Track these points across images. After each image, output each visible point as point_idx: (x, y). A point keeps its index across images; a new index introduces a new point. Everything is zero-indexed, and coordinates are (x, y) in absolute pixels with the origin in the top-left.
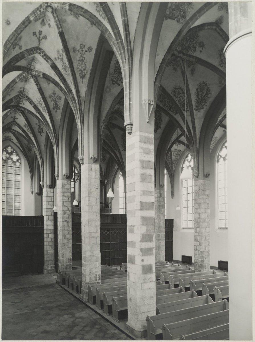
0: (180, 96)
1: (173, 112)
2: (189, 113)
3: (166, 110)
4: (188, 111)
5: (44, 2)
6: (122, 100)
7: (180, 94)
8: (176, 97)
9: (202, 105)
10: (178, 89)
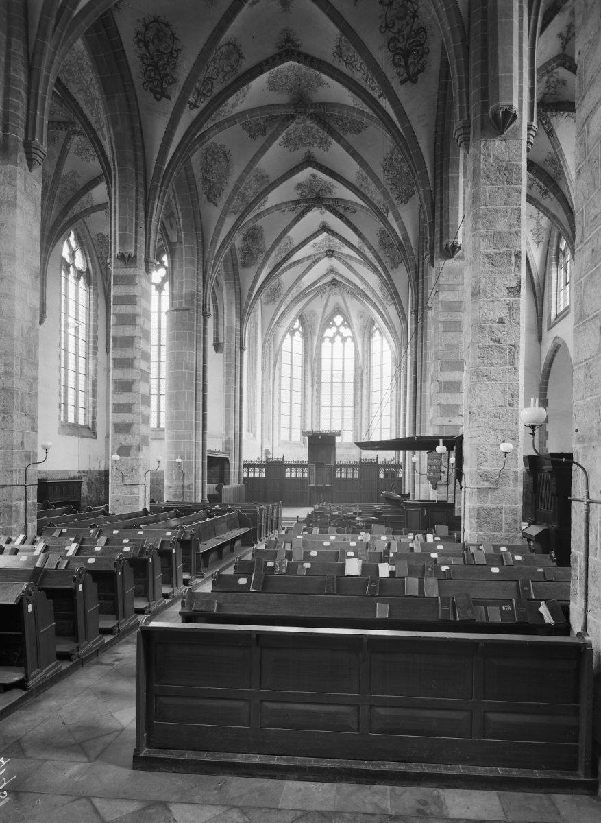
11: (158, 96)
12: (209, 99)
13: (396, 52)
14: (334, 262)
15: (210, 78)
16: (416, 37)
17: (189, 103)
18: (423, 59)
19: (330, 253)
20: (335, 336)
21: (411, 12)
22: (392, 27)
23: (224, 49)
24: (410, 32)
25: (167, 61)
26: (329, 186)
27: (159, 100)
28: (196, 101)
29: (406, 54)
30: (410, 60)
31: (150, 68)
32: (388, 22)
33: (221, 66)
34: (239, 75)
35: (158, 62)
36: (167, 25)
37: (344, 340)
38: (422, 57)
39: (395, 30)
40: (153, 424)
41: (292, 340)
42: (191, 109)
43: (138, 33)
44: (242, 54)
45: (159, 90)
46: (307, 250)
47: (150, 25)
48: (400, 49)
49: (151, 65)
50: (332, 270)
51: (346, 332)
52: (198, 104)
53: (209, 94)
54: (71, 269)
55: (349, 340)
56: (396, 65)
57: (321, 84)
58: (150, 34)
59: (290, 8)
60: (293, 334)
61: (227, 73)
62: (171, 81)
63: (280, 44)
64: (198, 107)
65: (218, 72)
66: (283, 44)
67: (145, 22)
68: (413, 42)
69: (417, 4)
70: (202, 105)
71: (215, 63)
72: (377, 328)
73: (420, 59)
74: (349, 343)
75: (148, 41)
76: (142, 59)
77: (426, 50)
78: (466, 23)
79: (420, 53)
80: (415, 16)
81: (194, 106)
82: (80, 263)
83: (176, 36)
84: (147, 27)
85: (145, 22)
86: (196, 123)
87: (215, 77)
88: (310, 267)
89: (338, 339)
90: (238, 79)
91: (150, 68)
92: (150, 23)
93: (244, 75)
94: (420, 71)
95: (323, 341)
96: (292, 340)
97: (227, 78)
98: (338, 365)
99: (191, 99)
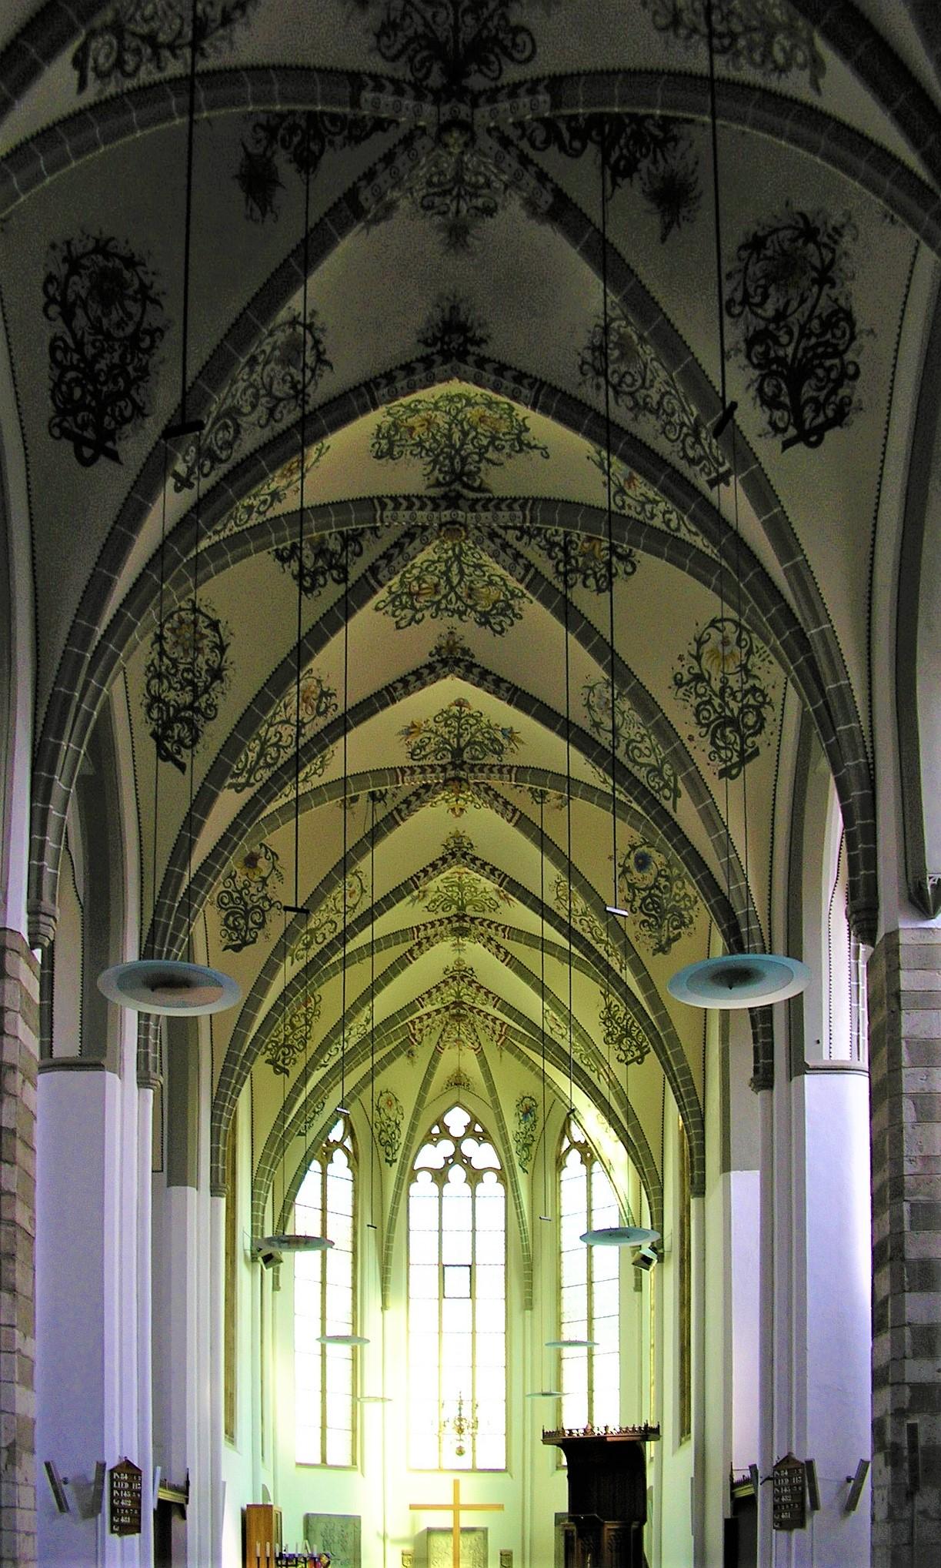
11: (87, 452)
12: (223, 469)
13: (766, 366)
14: (476, 954)
16: (823, 334)
17: (176, 475)
18: (843, 392)
19: (461, 925)
20: (447, 1166)
21: (814, 268)
22: (761, 305)
23: (281, 337)
24: (810, 318)
25: (122, 357)
26: (499, 736)
27: (86, 462)
28: (190, 471)
29: (796, 374)
30: (807, 391)
31: (71, 375)
32: (751, 290)
33: (266, 380)
35: (96, 358)
36: (130, 262)
37: (474, 1177)
38: (839, 383)
39: (769, 310)
41: (324, 1174)
42: (178, 490)
43: (50, 279)
44: (324, 352)
45: (89, 434)
46: (402, 915)
47: (85, 262)
48: (780, 361)
49: (73, 368)
50: (461, 974)
51: (483, 1155)
53: (223, 456)
55: (490, 1178)
56: (770, 402)
57: (521, 443)
58: (80, 286)
59: (469, 239)
60: (327, 1158)
61: (280, 400)
62: (127, 413)
63: (430, 334)
65: (256, 396)
66: (439, 335)
67: (69, 251)
68: (818, 345)
69: (833, 251)
70: (205, 484)
71: (252, 372)
72: (574, 1144)
73: (834, 392)
74: (491, 1185)
75: (74, 304)
76: (53, 349)
77: (851, 370)
78: (724, 312)
79: (834, 375)
80: (825, 277)
81: (183, 483)
83: (152, 293)
84: (74, 264)
85: (69, 251)
86: (185, 529)
87: (246, 409)
88: (402, 963)
89: (457, 1173)
91: (71, 375)
92: (83, 255)
93: (326, 407)
94: (830, 424)
95: (413, 1178)
96: (324, 1174)
97: (278, 416)
98: (457, 1250)
99: (181, 468)
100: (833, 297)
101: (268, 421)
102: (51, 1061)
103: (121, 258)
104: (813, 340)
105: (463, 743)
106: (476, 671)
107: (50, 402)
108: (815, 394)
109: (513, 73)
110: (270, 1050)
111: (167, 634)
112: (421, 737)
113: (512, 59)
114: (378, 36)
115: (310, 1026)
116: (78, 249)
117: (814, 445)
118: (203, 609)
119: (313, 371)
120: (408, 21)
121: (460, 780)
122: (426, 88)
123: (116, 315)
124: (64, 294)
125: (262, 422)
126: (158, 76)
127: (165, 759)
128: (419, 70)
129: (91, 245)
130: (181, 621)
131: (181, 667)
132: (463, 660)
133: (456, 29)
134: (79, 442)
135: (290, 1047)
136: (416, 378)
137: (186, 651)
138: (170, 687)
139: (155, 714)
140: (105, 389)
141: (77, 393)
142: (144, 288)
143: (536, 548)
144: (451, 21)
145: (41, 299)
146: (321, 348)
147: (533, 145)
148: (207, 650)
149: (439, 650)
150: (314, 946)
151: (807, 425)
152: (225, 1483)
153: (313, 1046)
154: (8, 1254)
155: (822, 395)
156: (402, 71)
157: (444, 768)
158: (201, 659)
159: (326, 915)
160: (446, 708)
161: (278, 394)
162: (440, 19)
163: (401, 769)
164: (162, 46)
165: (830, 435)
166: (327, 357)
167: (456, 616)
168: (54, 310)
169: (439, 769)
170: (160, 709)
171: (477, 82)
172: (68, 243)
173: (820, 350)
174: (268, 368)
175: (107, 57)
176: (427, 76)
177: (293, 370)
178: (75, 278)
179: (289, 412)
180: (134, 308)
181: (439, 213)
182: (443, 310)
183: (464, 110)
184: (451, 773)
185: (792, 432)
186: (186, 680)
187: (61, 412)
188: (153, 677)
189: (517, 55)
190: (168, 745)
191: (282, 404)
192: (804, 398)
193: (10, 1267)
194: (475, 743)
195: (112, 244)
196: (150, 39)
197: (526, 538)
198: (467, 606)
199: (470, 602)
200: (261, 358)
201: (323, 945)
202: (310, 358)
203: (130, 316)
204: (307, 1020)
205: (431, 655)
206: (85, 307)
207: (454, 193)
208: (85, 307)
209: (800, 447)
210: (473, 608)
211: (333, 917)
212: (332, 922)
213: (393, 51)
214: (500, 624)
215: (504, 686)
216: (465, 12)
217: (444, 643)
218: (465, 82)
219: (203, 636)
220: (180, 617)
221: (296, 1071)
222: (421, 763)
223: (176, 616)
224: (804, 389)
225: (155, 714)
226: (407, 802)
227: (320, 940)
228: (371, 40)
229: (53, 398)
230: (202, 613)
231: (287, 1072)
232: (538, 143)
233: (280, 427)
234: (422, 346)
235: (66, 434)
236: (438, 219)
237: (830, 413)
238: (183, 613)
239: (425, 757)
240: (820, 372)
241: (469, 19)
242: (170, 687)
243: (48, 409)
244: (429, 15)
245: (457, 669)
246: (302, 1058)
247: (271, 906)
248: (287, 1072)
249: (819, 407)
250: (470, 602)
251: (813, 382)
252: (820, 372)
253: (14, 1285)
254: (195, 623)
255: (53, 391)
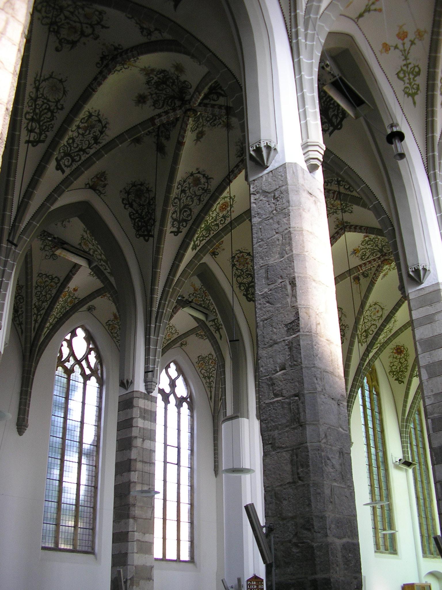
0: (83, 135)
1: (31, 131)
2: (59, 176)
3: (25, 111)
4: (63, 172)
5: (253, 277)
6: (26, 54)
7: (88, 132)
8: (78, 127)
9: (261, 314)
10: (100, 121)
12: (191, 222)
15: (186, 206)
25: (148, 209)
28: (179, 228)
31: (137, 220)
33: (193, 193)
34: (211, 193)
36: (142, 184)
40: (158, 553)
43: (123, 200)
44: (208, 176)
45: (146, 233)
47: (131, 191)
49: (137, 218)
52: (180, 230)
54: (172, 398)
58: (132, 197)
61: (200, 195)
63: (239, 154)
64: (181, 232)
65: (192, 198)
71: (185, 194)
76: (130, 216)
82: (181, 390)
84: (128, 193)
87: (191, 203)
90: (211, 196)
92: (130, 189)
94: (342, 119)
97: (202, 200)
100: (322, 83)
101: (200, 202)
102: (226, 418)
103: (139, 185)
104: (324, 99)
105: (381, 247)
106: (353, 227)
107: (134, 229)
108: (333, 113)
109: (192, 91)
110: (395, 375)
111: (236, 263)
112: (361, 252)
113: (189, 88)
114: (154, 105)
115: (407, 361)
116: (127, 189)
117: (340, 129)
118: (243, 251)
119: (207, 182)
120: (160, 98)
121: (387, 260)
122: (177, 107)
123: (143, 199)
124: (128, 201)
125: (198, 203)
126: (88, 156)
127: (249, 301)
128: (172, 104)
129: (131, 186)
130: (239, 257)
131: (245, 271)
132: (347, 226)
133: (173, 90)
134: (144, 236)
135: (402, 371)
136: (240, 167)
137: (244, 265)
138: (244, 278)
139: (242, 288)
140: (146, 219)
141: (140, 224)
142: (147, 189)
143: (334, 185)
144: (171, 90)
145: (123, 205)
146: (206, 176)
147: (214, 100)
148: (250, 263)
149: (337, 226)
150: (370, 336)
151: (335, 124)
152: (365, 577)
153: (410, 368)
154: (133, 504)
155: (336, 112)
156: (166, 108)
157: (379, 258)
158: (249, 266)
159: (369, 323)
160: (363, 240)
161: (198, 194)
162: (168, 91)
163: (360, 265)
164: (85, 149)
165: (344, 123)
166: (209, 177)
167: (335, 214)
168: (127, 206)
169: (377, 259)
170: (243, 286)
171: (188, 97)
172: (125, 189)
173: (328, 100)
174: (191, 190)
175: (68, 162)
176: (175, 104)
177: (200, 186)
178: (130, 196)
179: (206, 197)
180: (147, 195)
181: (219, 125)
182: (239, 145)
183: (188, 106)
184: (382, 259)
185: (331, 128)
186: (247, 274)
187: (137, 231)
188: (237, 277)
189: (189, 87)
190: (249, 296)
191: (202, 196)
192: (331, 116)
193: (133, 509)
194: (384, 246)
195: (136, 182)
196: (81, 150)
197: (329, 184)
198: (335, 209)
199: (335, 208)
200: (186, 189)
201: (373, 334)
202: (203, 180)
203: (147, 198)
204: (405, 359)
205: (335, 229)
206: (135, 201)
207: (218, 118)
208: (135, 201)
209: (336, 131)
210: (337, 209)
211: (374, 323)
212: (374, 325)
213: (161, 105)
214: (349, 209)
215: (363, 228)
216: (172, 86)
217: (337, 223)
218: (186, 99)
219: (247, 259)
220: (237, 256)
221: (406, 381)
222: (368, 260)
223: (236, 257)
224: (330, 113)
225: (242, 288)
226: (375, 274)
227: (371, 332)
228: (153, 108)
229: (134, 228)
230: (244, 252)
231: (403, 382)
232: (215, 99)
233: (204, 202)
234: (238, 158)
235: (140, 236)
236: (220, 126)
237: (341, 116)
238: (238, 255)
239: (368, 258)
240: (331, 106)
241: (174, 87)
242: (244, 278)
243: (134, 231)
244: (164, 92)
245: (346, 229)
246: (407, 374)
247: (345, 327)
248: (403, 382)
249: (336, 116)
250: (335, 208)
251: (331, 110)
252: (331, 106)
253: (135, 516)
254: (243, 256)
255: (134, 226)
